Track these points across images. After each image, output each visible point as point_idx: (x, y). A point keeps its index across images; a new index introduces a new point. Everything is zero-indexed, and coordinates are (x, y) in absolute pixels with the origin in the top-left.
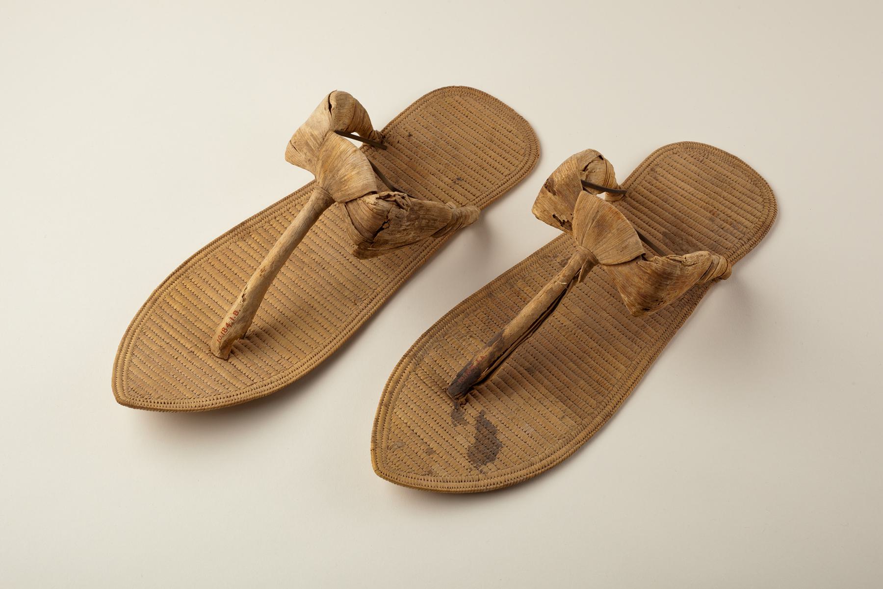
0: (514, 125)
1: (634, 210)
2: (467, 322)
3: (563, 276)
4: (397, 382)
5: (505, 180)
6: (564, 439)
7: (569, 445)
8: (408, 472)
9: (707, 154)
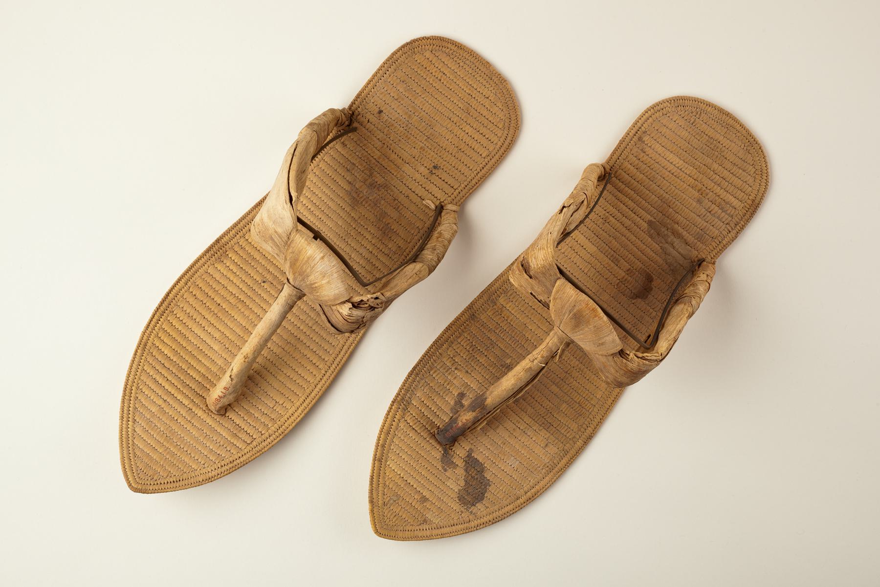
1: (620, 194)
2: (451, 353)
3: (541, 357)
4: (388, 433)
5: (484, 163)
6: (547, 469)
7: (552, 473)
8: (405, 526)
9: (699, 113)
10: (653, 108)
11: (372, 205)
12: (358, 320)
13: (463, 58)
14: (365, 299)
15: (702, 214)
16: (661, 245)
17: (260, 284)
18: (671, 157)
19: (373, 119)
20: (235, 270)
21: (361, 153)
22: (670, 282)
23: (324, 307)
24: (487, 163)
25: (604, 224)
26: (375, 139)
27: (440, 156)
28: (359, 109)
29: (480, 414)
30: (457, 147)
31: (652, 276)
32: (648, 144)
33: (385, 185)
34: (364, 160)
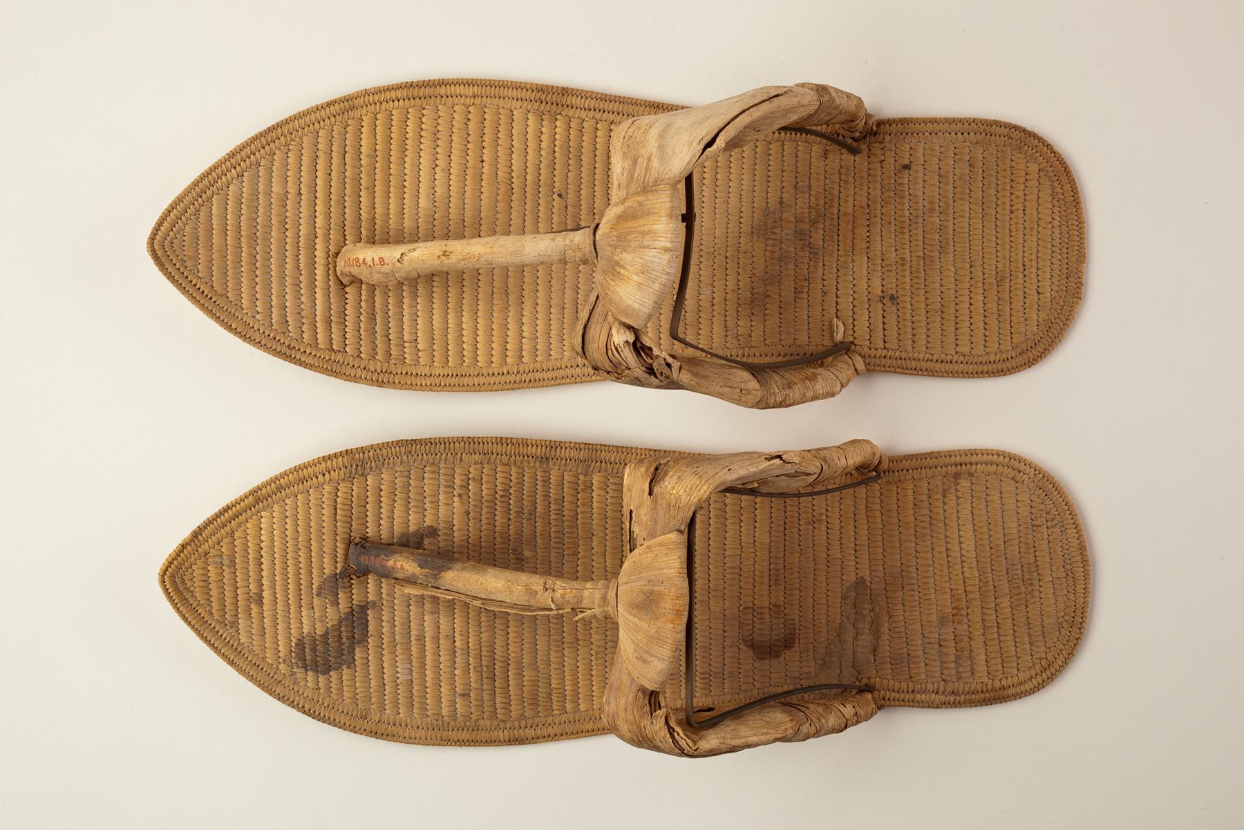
0: (1057, 288)
3: (561, 595)
5: (949, 358)
9: (1055, 522)
10: (1010, 459)
11: (777, 255)
12: (620, 364)
13: (1064, 218)
14: (656, 352)
15: (929, 638)
16: (844, 619)
17: (554, 193)
18: (968, 533)
19: (890, 165)
20: (544, 145)
21: (832, 186)
22: (807, 673)
23: (600, 304)
24: (954, 361)
25: (808, 523)
26: (865, 188)
27: (912, 293)
28: (888, 138)
29: (424, 578)
30: (942, 305)
31: (794, 643)
32: (959, 491)
33: (816, 251)
34: (825, 198)
